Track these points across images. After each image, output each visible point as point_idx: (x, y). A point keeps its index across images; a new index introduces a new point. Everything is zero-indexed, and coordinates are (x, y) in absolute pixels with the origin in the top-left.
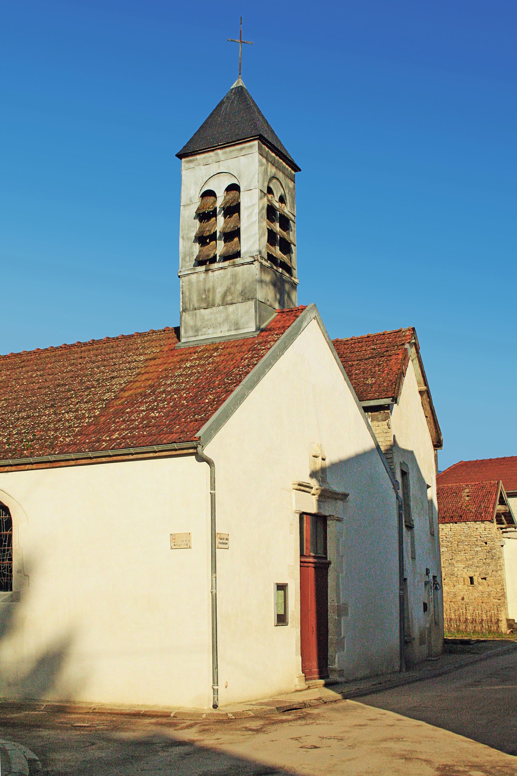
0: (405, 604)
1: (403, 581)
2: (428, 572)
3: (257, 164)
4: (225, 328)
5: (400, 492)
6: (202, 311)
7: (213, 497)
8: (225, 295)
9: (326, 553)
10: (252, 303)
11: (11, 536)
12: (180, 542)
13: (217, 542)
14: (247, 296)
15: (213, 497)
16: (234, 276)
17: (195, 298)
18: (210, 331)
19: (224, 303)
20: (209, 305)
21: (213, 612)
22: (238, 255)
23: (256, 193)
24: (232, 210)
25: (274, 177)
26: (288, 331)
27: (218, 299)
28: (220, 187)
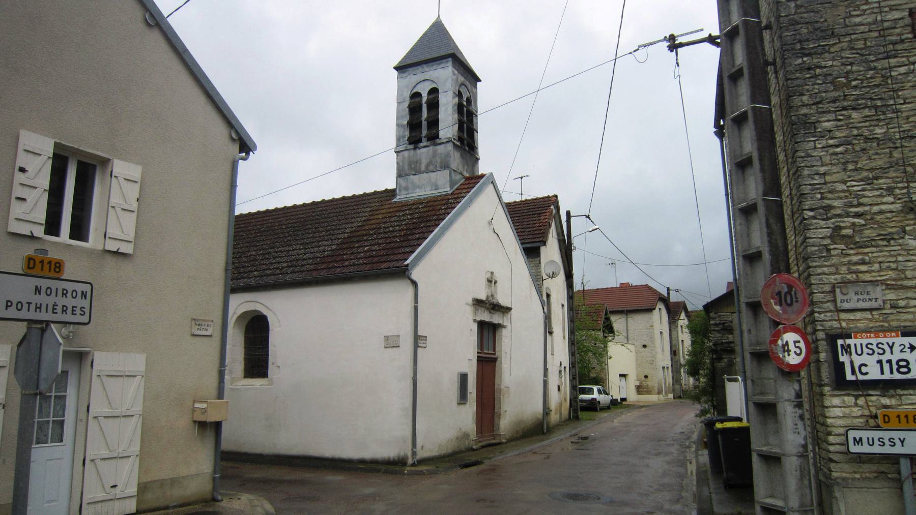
0: (765, 235)
1: (546, 370)
2: (561, 364)
3: (451, 74)
4: (429, 189)
5: (546, 310)
6: (412, 177)
7: (416, 308)
8: (428, 166)
9: (494, 350)
10: (447, 172)
11: (397, 119)
12: (391, 343)
13: (418, 340)
14: (445, 166)
15: (416, 308)
16: (435, 154)
17: (406, 167)
18: (417, 190)
19: (427, 171)
20: (417, 172)
21: (412, 393)
22: (437, 137)
23: (450, 94)
24: (434, 105)
25: (463, 84)
26: (473, 190)
27: (423, 169)
28: (424, 90)
